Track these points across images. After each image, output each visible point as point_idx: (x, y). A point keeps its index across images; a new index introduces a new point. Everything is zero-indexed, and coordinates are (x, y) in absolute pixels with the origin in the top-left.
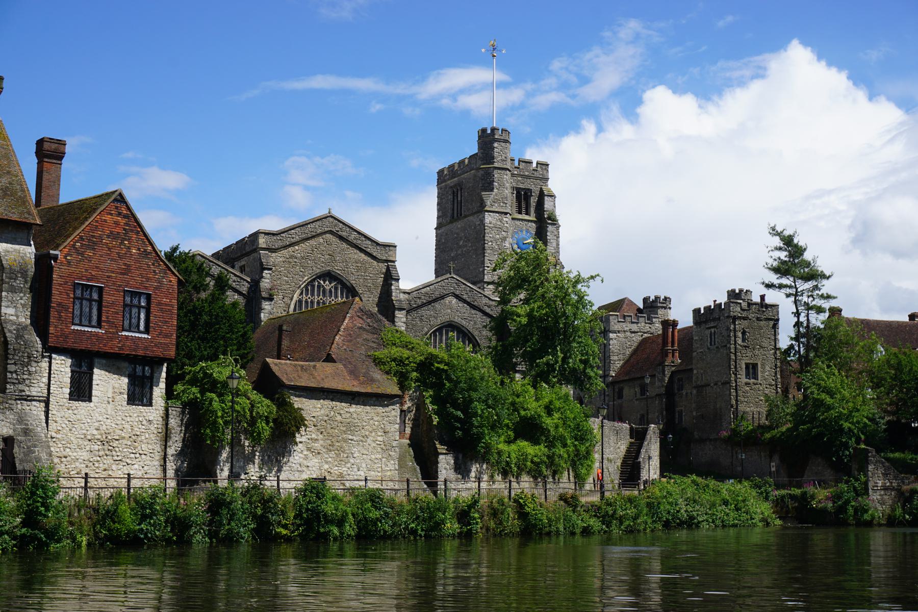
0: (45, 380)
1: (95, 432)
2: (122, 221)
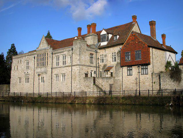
0: (122, 73)
1: (134, 82)
2: (133, 37)
